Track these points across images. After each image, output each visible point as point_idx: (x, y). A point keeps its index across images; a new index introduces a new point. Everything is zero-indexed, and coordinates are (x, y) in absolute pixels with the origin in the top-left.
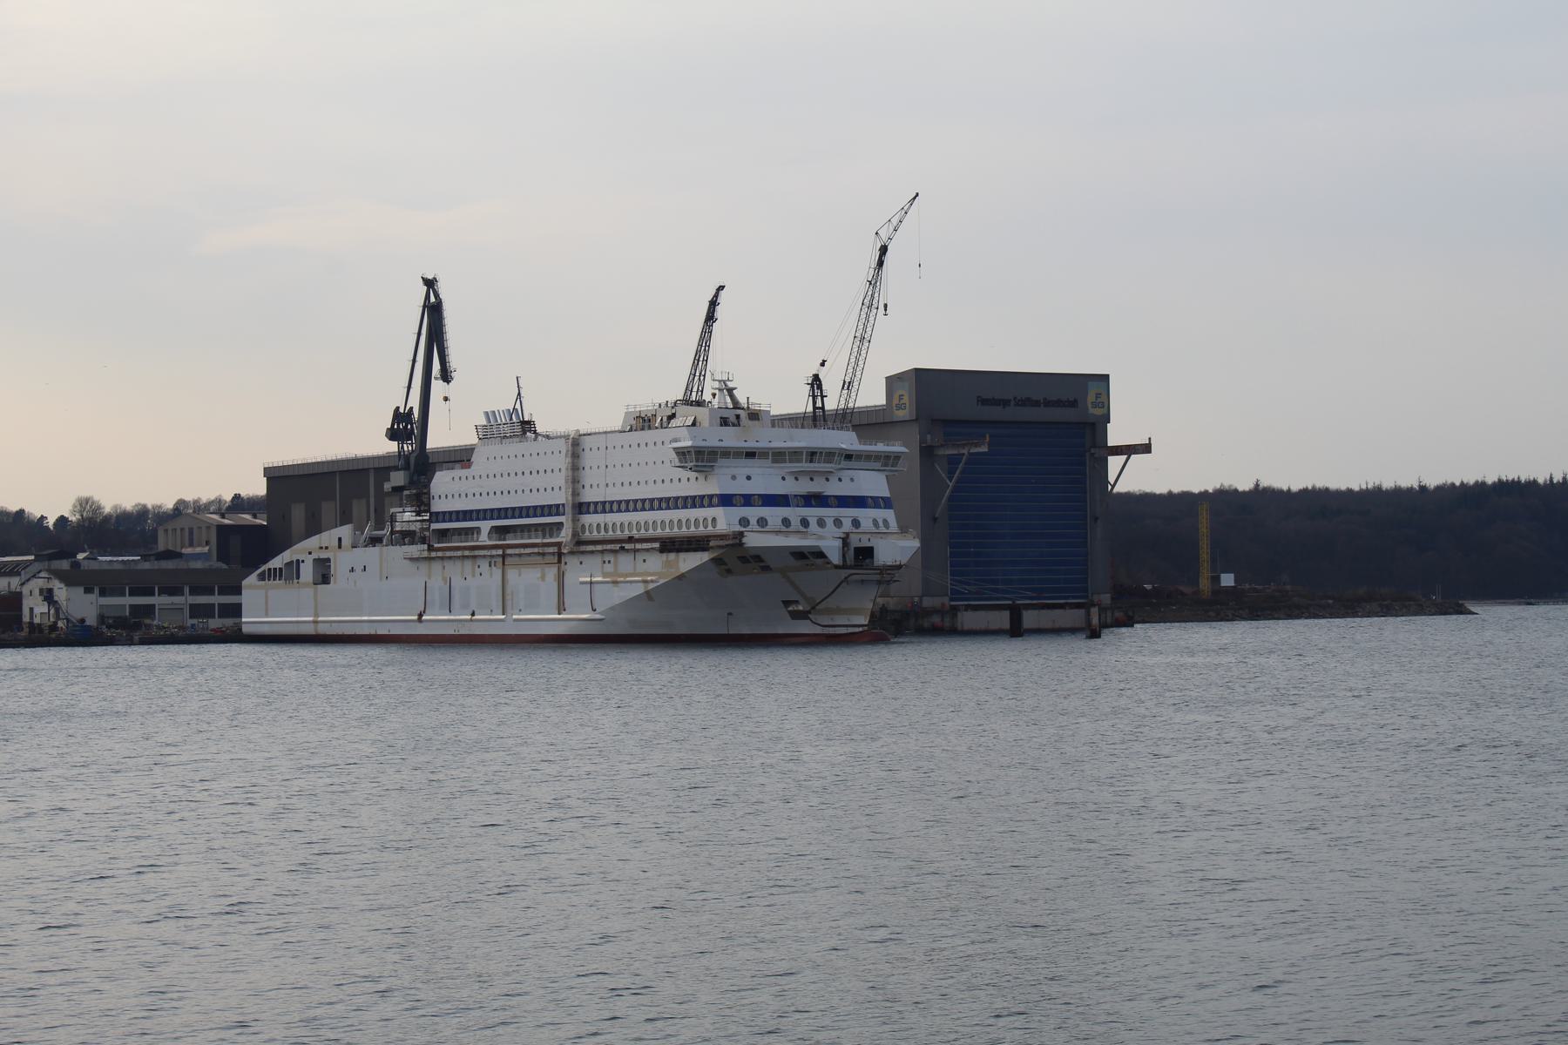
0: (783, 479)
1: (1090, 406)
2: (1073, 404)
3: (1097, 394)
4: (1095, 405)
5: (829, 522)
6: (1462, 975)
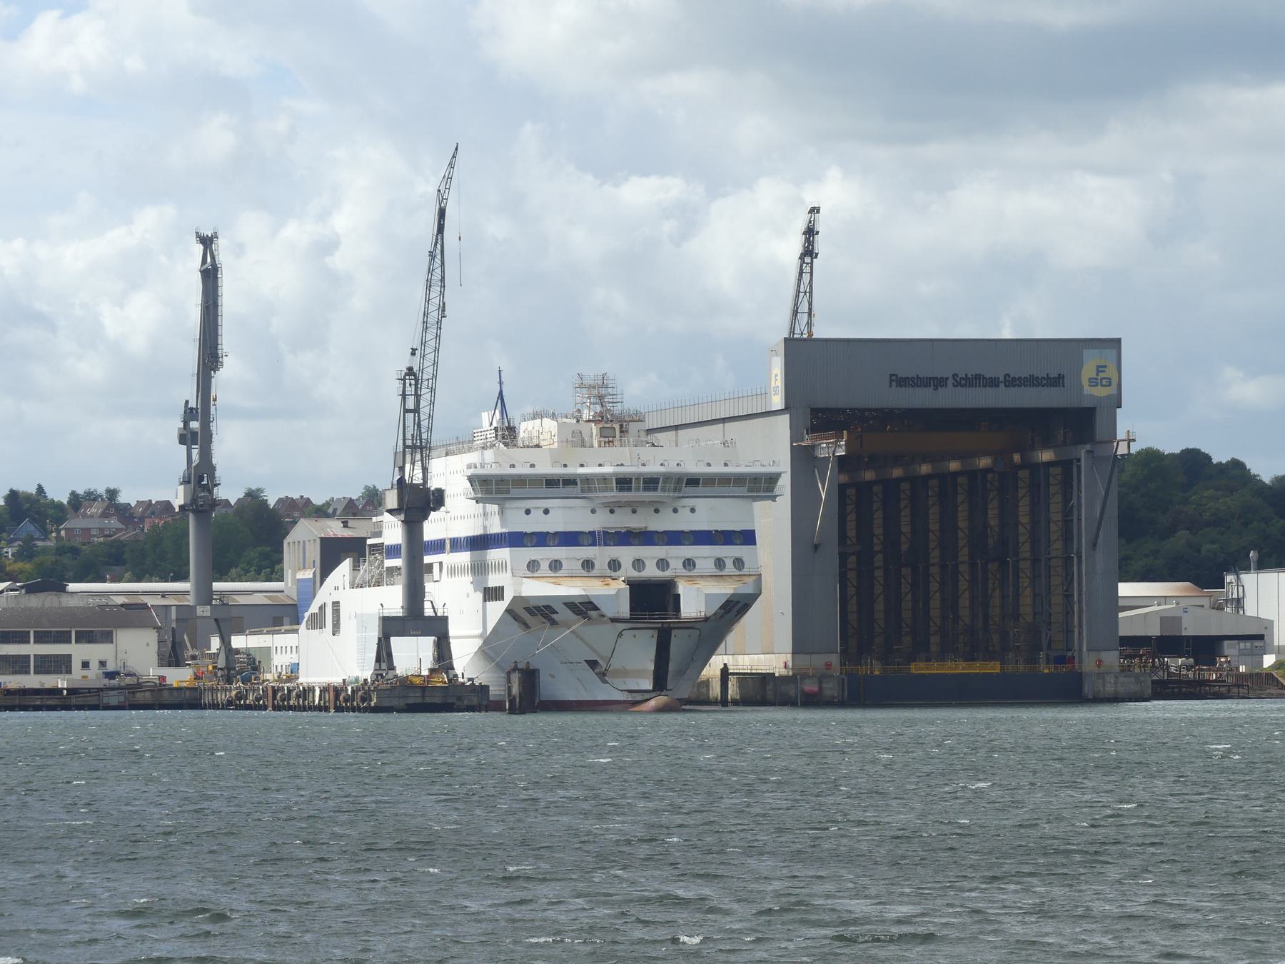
0: (593, 511)
1: (1085, 383)
2: (1057, 381)
3: (1098, 367)
4: (1093, 382)
5: (729, 564)
6: (1198, 903)
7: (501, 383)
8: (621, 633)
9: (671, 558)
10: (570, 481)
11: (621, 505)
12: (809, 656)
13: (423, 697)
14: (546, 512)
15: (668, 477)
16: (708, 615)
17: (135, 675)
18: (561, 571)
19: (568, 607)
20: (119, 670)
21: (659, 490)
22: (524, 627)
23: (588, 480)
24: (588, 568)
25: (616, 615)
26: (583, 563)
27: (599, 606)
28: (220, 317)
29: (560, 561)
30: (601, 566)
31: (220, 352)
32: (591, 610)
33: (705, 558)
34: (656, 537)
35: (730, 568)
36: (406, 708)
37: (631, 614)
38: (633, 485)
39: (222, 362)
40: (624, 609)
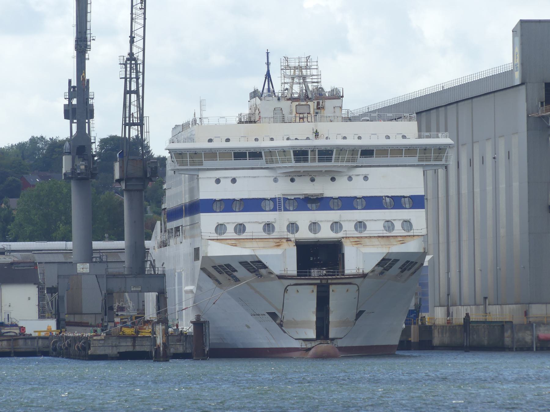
0: (276, 180)
5: (398, 225)
7: (268, 64)
8: (286, 288)
9: (345, 221)
10: (255, 154)
11: (301, 174)
12: (544, 306)
13: (134, 346)
14: (234, 181)
15: (341, 150)
16: (366, 271)
17: (16, 325)
18: (245, 234)
19: (243, 265)
20: (3, 321)
21: (333, 160)
22: (217, 283)
23: (271, 152)
24: (269, 231)
25: (283, 273)
26: (264, 226)
27: (267, 265)
28: (89, 5)
29: (244, 225)
30: (281, 229)
31: (88, 36)
32: (261, 268)
33: (375, 220)
34: (331, 203)
35: (230, 233)
36: (118, 355)
37: (298, 272)
38: (309, 157)
39: (90, 45)
40: (292, 268)
